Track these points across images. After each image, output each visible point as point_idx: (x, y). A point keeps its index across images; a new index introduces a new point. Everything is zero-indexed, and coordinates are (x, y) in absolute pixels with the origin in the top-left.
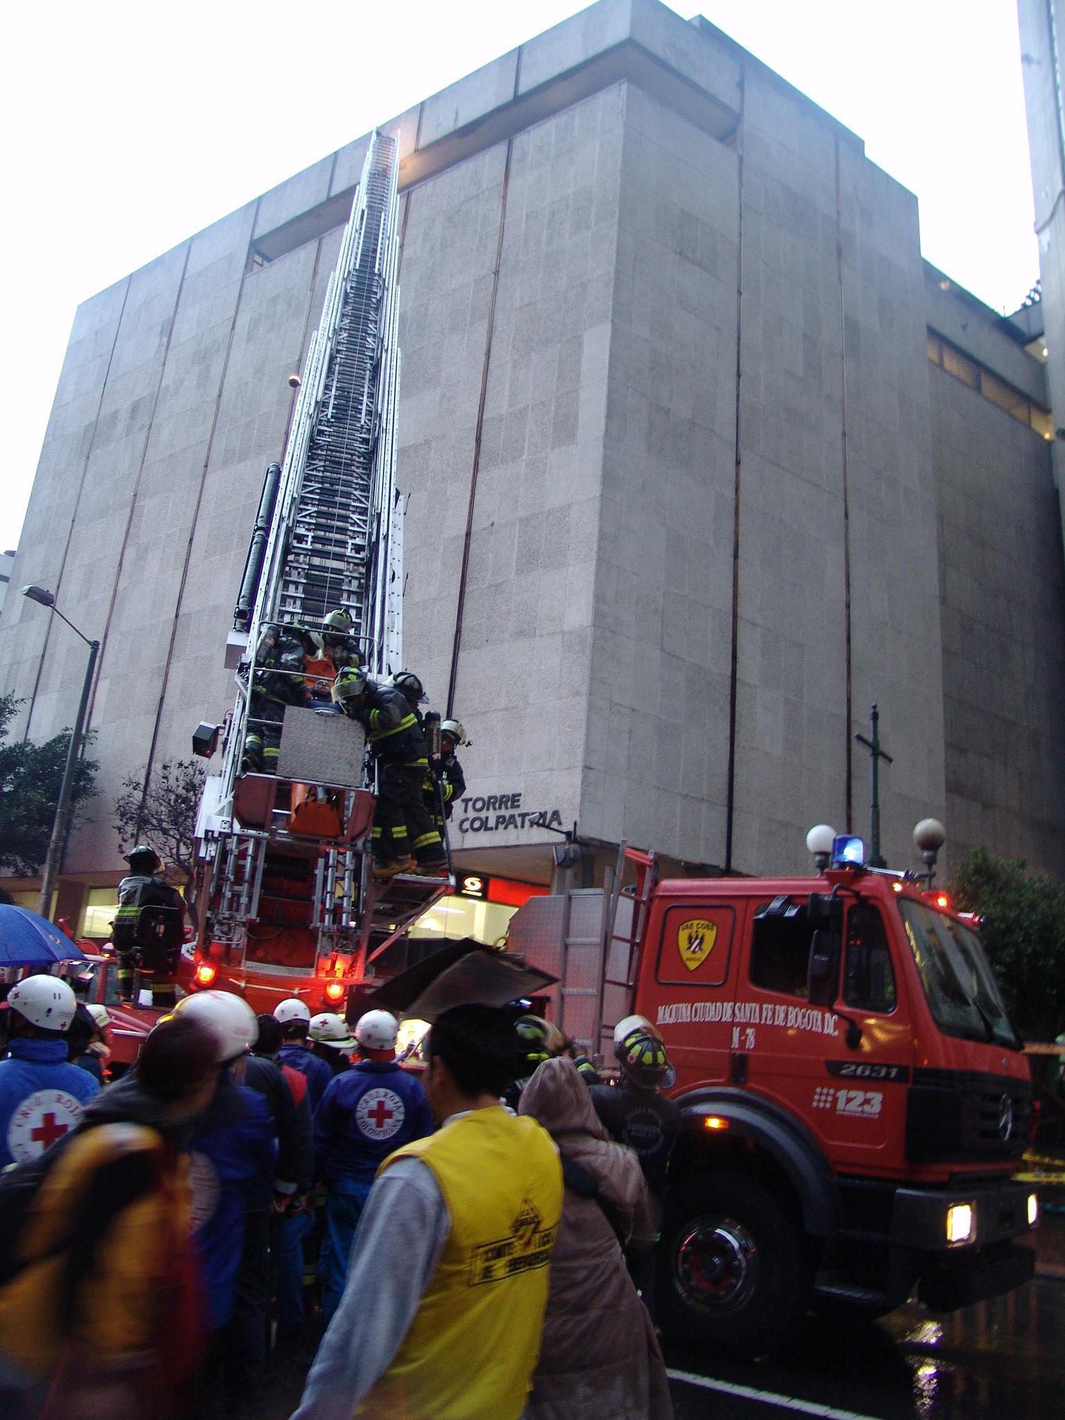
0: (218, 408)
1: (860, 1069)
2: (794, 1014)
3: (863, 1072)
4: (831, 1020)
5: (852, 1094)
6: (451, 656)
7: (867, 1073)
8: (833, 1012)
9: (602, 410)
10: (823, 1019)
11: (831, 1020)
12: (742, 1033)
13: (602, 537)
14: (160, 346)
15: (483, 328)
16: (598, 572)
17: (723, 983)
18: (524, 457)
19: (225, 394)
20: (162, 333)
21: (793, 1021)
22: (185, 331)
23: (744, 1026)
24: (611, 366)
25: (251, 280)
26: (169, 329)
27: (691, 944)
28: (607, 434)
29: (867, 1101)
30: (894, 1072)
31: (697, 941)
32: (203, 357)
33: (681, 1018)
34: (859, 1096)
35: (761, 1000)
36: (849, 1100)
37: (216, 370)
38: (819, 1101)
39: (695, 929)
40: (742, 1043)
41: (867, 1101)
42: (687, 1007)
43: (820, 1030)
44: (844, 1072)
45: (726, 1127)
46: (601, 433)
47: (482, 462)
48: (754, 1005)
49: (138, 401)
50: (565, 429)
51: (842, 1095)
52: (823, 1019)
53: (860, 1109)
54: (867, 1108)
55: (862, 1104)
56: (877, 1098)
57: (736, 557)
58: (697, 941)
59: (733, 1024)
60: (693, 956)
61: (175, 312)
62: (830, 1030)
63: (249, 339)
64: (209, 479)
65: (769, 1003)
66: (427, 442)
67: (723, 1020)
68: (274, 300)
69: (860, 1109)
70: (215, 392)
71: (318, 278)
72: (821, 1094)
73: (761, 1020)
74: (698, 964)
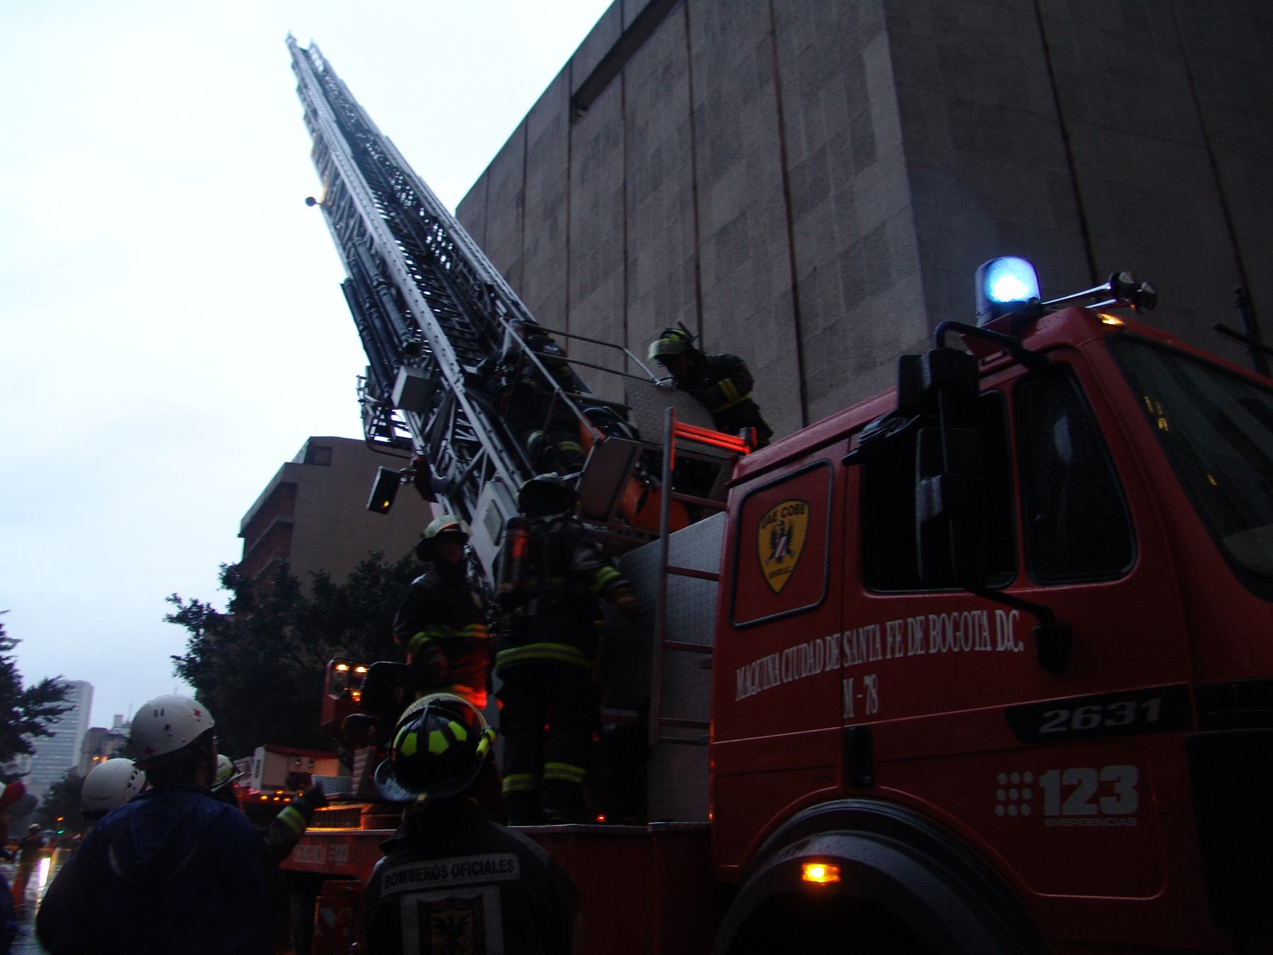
0: (569, 251)
1: (1078, 716)
2: (939, 626)
3: (1086, 721)
4: (1006, 619)
5: (1071, 776)
6: (800, 412)
7: (1096, 720)
8: (1010, 603)
9: (895, 119)
10: (992, 619)
11: (1006, 619)
12: (859, 688)
13: (921, 245)
14: (518, 216)
15: (770, 88)
16: (924, 281)
17: (823, 602)
18: (831, 194)
19: (572, 237)
20: (517, 204)
21: (939, 640)
22: (534, 196)
23: (858, 672)
24: (896, 72)
25: (577, 130)
26: (522, 200)
27: (774, 545)
28: (906, 141)
29: (1106, 789)
30: (1154, 706)
31: (784, 539)
32: (550, 213)
33: (769, 683)
34: (1087, 778)
35: (880, 614)
36: (1066, 792)
37: (562, 219)
38: (1007, 802)
39: (779, 518)
40: (859, 705)
41: (1106, 789)
42: (774, 659)
43: (989, 648)
44: (1045, 729)
45: (835, 878)
46: (899, 141)
47: (794, 213)
48: (871, 627)
49: (509, 270)
50: (864, 150)
51: (1050, 780)
52: (992, 619)
53: (1092, 809)
54: (1108, 805)
55: (1094, 799)
56: (1126, 776)
57: (1085, 233)
58: (784, 539)
59: (842, 673)
60: (780, 566)
61: (525, 183)
62: (1007, 643)
63: (583, 181)
64: (573, 315)
65: (769, 586)
66: (743, 213)
67: (828, 669)
68: (596, 140)
69: (1092, 809)
70: (564, 239)
71: (627, 106)
72: (1008, 787)
73: (884, 653)
74: (785, 577)
